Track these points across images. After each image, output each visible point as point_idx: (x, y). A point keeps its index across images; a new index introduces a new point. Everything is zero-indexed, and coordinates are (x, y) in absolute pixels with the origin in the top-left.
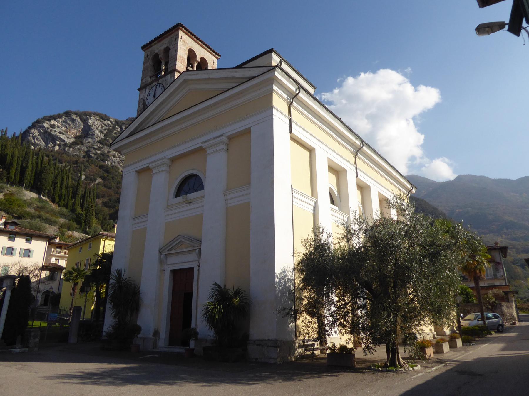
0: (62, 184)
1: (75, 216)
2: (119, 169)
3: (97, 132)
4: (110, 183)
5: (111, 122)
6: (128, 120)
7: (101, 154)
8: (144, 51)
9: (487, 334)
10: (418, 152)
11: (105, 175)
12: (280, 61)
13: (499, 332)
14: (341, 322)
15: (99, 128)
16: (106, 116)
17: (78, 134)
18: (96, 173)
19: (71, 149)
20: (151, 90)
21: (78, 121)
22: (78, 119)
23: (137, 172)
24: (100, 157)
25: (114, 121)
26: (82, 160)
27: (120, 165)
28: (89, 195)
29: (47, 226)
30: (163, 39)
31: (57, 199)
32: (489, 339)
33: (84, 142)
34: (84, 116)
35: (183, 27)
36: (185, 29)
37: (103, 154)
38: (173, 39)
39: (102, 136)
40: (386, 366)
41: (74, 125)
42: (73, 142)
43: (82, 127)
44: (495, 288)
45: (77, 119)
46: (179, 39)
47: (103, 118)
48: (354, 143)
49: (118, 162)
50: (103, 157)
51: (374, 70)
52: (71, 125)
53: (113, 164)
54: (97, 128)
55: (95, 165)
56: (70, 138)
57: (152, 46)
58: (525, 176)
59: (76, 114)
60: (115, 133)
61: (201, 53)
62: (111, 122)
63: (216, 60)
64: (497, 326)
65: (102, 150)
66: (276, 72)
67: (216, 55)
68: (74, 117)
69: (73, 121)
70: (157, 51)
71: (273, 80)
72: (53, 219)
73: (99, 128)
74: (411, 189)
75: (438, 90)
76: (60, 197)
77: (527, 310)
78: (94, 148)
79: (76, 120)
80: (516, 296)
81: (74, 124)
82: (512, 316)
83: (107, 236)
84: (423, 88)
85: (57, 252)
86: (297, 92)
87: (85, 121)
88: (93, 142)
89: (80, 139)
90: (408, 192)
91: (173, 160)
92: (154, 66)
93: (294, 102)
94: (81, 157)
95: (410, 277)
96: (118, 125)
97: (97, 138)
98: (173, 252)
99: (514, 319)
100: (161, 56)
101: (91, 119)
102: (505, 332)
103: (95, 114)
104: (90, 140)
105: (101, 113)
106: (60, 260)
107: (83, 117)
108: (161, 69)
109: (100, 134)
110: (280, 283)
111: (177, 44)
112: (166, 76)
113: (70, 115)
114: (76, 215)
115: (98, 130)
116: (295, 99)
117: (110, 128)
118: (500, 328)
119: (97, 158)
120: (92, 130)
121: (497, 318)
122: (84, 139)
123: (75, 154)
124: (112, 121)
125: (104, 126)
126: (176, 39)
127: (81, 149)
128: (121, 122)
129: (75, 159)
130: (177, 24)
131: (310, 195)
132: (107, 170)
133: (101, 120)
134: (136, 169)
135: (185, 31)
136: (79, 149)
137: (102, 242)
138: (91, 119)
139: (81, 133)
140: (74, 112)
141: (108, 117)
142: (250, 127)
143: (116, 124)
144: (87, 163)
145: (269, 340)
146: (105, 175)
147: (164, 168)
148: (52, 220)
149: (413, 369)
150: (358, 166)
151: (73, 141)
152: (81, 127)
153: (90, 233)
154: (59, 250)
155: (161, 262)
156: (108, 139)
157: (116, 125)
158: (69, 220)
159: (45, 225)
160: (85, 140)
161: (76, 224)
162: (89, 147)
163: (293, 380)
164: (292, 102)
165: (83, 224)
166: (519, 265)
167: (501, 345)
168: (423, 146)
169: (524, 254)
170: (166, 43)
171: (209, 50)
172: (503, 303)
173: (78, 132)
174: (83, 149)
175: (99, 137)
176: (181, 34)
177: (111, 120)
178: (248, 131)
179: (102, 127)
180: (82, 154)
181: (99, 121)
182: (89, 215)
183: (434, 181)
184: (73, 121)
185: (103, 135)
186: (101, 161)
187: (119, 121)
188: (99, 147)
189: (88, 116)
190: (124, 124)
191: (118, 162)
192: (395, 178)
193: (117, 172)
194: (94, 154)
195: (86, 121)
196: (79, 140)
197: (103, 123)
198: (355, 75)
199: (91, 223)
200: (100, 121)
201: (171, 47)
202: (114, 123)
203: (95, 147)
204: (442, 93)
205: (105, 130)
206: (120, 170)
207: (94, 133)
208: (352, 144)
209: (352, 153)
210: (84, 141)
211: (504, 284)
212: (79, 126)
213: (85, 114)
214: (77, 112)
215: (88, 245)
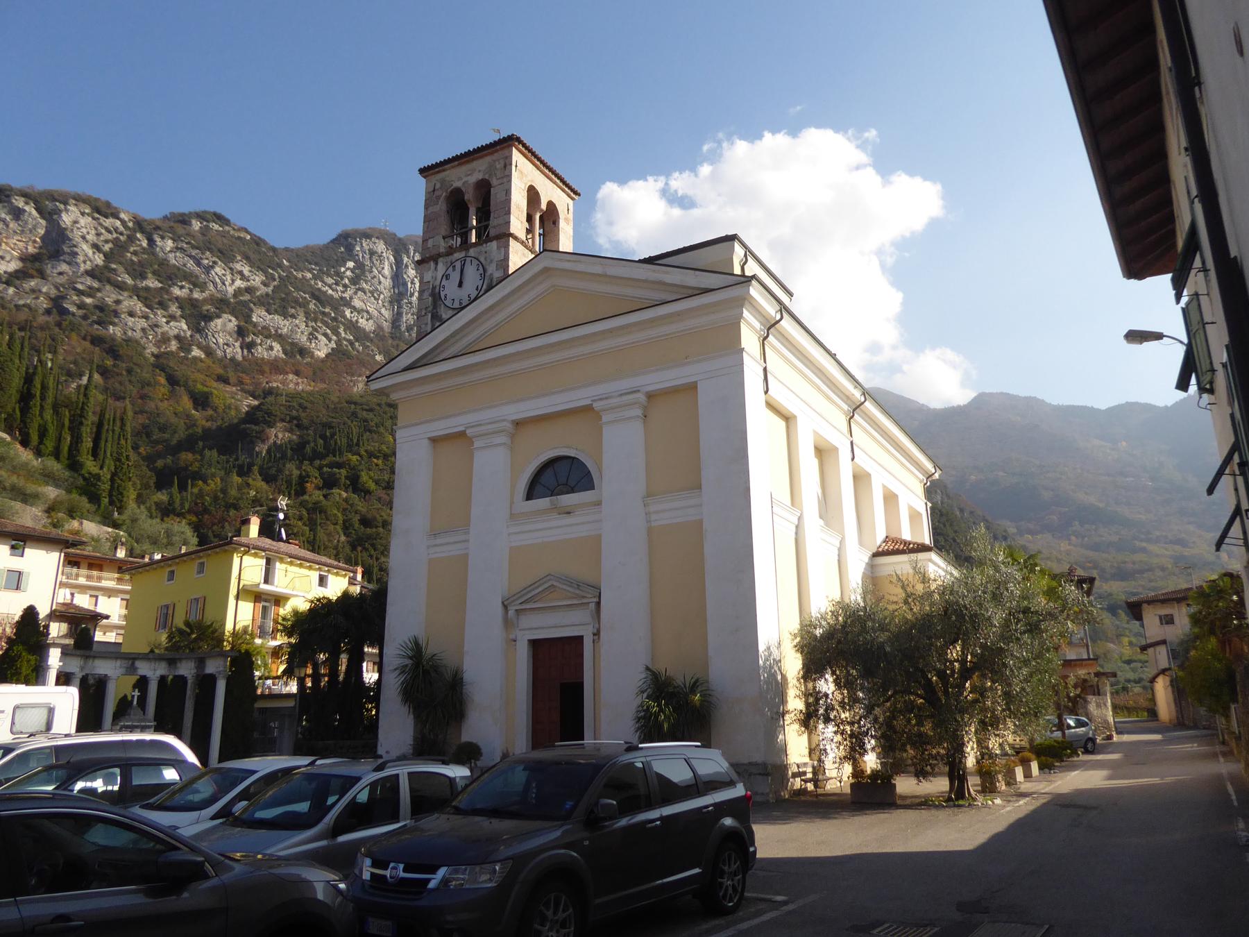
0: (43, 398)
1: (81, 482)
2: (145, 348)
3: (85, 247)
4: (121, 383)
5: (123, 222)
6: (169, 219)
7: (96, 307)
8: (425, 177)
9: (1070, 756)
10: (889, 335)
11: (109, 363)
12: (745, 255)
13: (1087, 752)
14: (426, 747)
15: (91, 237)
16: (108, 204)
17: (31, 250)
18: (85, 356)
19: (11, 290)
20: (451, 268)
21: (30, 214)
22: (30, 209)
23: (434, 440)
24: (93, 314)
25: (130, 220)
26: (42, 319)
27: (148, 338)
28: (111, 428)
29: (18, 505)
30: (473, 160)
31: (35, 438)
32: (1077, 763)
33: (48, 272)
34: (49, 204)
35: (519, 140)
36: (524, 145)
37: (101, 308)
38: (499, 166)
39: (99, 260)
40: (950, 799)
41: (19, 225)
42: (16, 271)
43: (42, 232)
44: (1081, 666)
45: (27, 208)
46: (514, 168)
47: (101, 209)
48: (850, 397)
49: (143, 330)
50: (101, 314)
51: (794, 131)
52: (11, 225)
53: (130, 333)
54: (84, 238)
55: (79, 335)
56: (8, 258)
57: (444, 170)
58: (1127, 402)
59: (26, 195)
60: (135, 253)
61: (550, 192)
62: (123, 222)
63: (571, 202)
64: (1084, 741)
65: (99, 295)
66: (751, 288)
67: (572, 194)
68: (20, 202)
69: (17, 214)
70: (458, 184)
71: (744, 300)
72: (31, 488)
73: (91, 237)
74: (933, 471)
75: (939, 187)
76: (43, 434)
77: (1125, 710)
78: (75, 289)
79: (25, 211)
80: (1113, 679)
81: (20, 223)
82: (1106, 722)
83: (249, 547)
84: (902, 181)
85: (89, 578)
86: (778, 317)
87: (50, 216)
88: (74, 272)
89: (37, 265)
90: (927, 478)
92: (448, 212)
93: (770, 336)
94: (41, 311)
95: (1004, 664)
96: (143, 231)
97: (85, 262)
98: (528, 606)
99: (1110, 730)
100: (469, 196)
101: (67, 211)
102: (1099, 753)
103: (80, 199)
104: (64, 267)
105: (95, 195)
106: (100, 598)
107: (47, 205)
108: (469, 226)
109: (94, 253)
110: (765, 668)
111: (509, 176)
112: (486, 243)
113: (8, 196)
114: (85, 479)
115: (87, 242)
116: (772, 330)
117: (121, 237)
118: (1090, 745)
119: (85, 317)
120: (70, 240)
121: (1083, 726)
122: (47, 264)
123: (21, 302)
124: (126, 219)
125: (103, 231)
126: (505, 166)
127: (40, 291)
128: (150, 222)
129: (22, 316)
130: (508, 136)
131: (788, 502)
132: (112, 349)
133: (97, 215)
135: (523, 149)
136: (33, 291)
137: (236, 560)
138: (67, 211)
139: (40, 248)
140: (20, 191)
141: (116, 208)
142: (696, 382)
143: (137, 227)
144: (57, 330)
145: (750, 764)
146: (109, 363)
147: (502, 439)
148: (28, 492)
149: (993, 803)
150: (855, 439)
151: (18, 268)
152: (39, 231)
153: (122, 525)
154: (75, 570)
155: (508, 624)
156: (114, 266)
157: (136, 232)
158: (69, 491)
159: (13, 503)
160: (49, 266)
161: (87, 500)
162: (63, 285)
163: (829, 818)
164: (768, 336)
165: (106, 501)
166: (1106, 606)
167: (1104, 773)
168: (905, 319)
169: (1117, 583)
170: (479, 171)
171: (561, 184)
172: (1090, 698)
173: (30, 243)
174: (44, 290)
175: (91, 261)
176: (517, 156)
177: (122, 216)
178: (692, 387)
179: (98, 235)
180: (43, 303)
181: (90, 219)
182: (121, 480)
183: (923, 405)
184: (17, 214)
185: (101, 255)
186: (96, 326)
187: (146, 221)
188: (90, 288)
189: (60, 202)
190: (157, 228)
191: (143, 330)
192: (909, 456)
193: (141, 355)
194: (76, 304)
195: (55, 217)
196: (33, 265)
197: (101, 224)
198: (753, 136)
199: (125, 499)
200: (94, 218)
201: (494, 182)
202: (131, 224)
203: (80, 286)
204: (949, 197)
205: (107, 241)
206: (148, 351)
207: (75, 249)
208: (847, 398)
209: (845, 413)
210: (48, 269)
211: (1085, 657)
212: (35, 227)
213: (52, 196)
214: (28, 191)
215: (194, 566)
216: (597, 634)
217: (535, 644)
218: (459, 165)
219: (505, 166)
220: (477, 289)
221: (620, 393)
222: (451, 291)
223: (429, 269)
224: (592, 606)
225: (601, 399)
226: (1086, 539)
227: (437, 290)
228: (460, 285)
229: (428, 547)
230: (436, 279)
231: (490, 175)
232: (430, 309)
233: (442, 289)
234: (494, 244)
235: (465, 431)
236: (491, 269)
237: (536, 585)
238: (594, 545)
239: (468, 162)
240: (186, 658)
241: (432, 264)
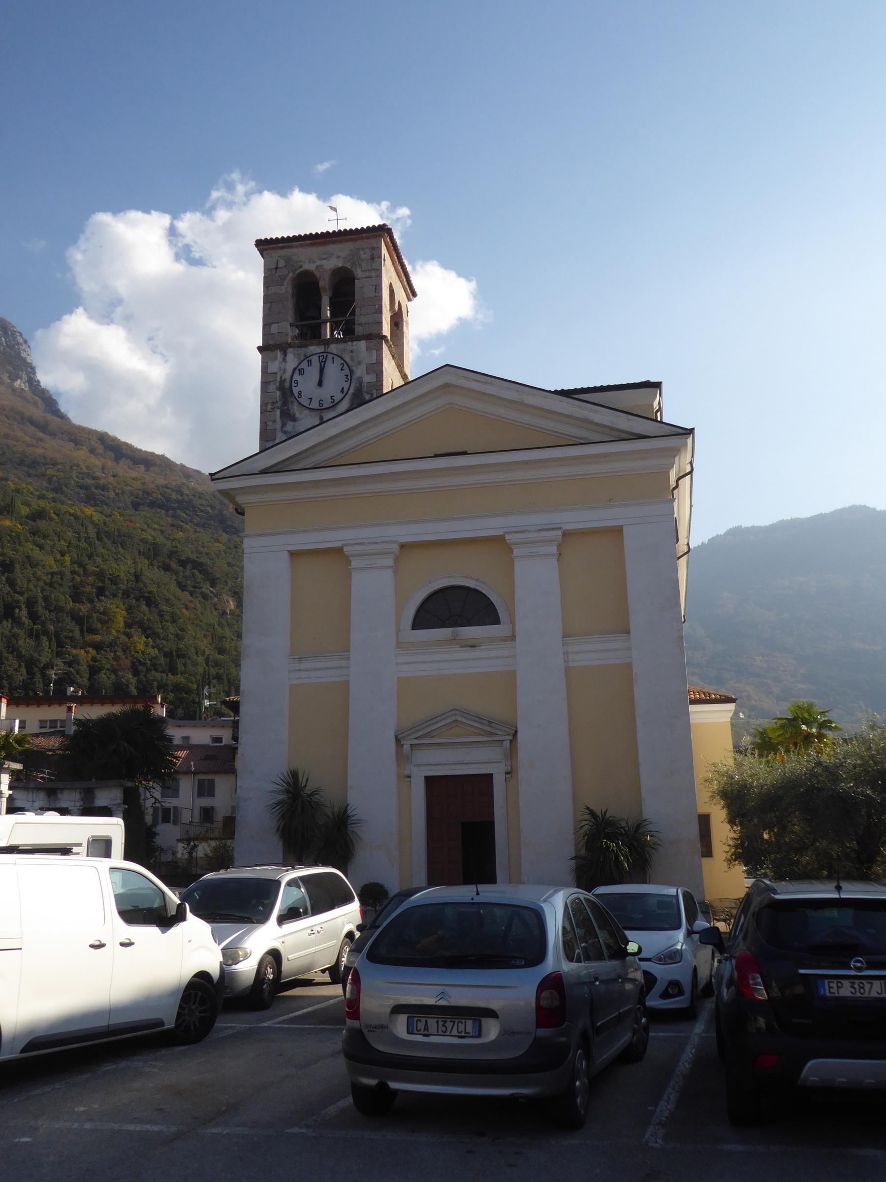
23: (293, 554)
38: (365, 255)
75: (435, 262)
91: (402, 546)
100: (324, 283)
126: (373, 258)
134: (290, 549)
142: (622, 526)
155: (402, 758)
171: (406, 283)
178: (618, 531)
201: (359, 273)
216: (509, 774)
217: (430, 781)
219: (373, 258)
220: (342, 391)
221: (539, 528)
222: (306, 385)
223: (276, 359)
224: (507, 744)
225: (516, 532)
227: (287, 384)
228: (320, 384)
229: (290, 671)
232: (279, 404)
233: (293, 384)
234: (363, 344)
235: (342, 547)
236: (360, 371)
237: (434, 721)
238: (510, 679)
239: (320, 244)
240: (69, 789)
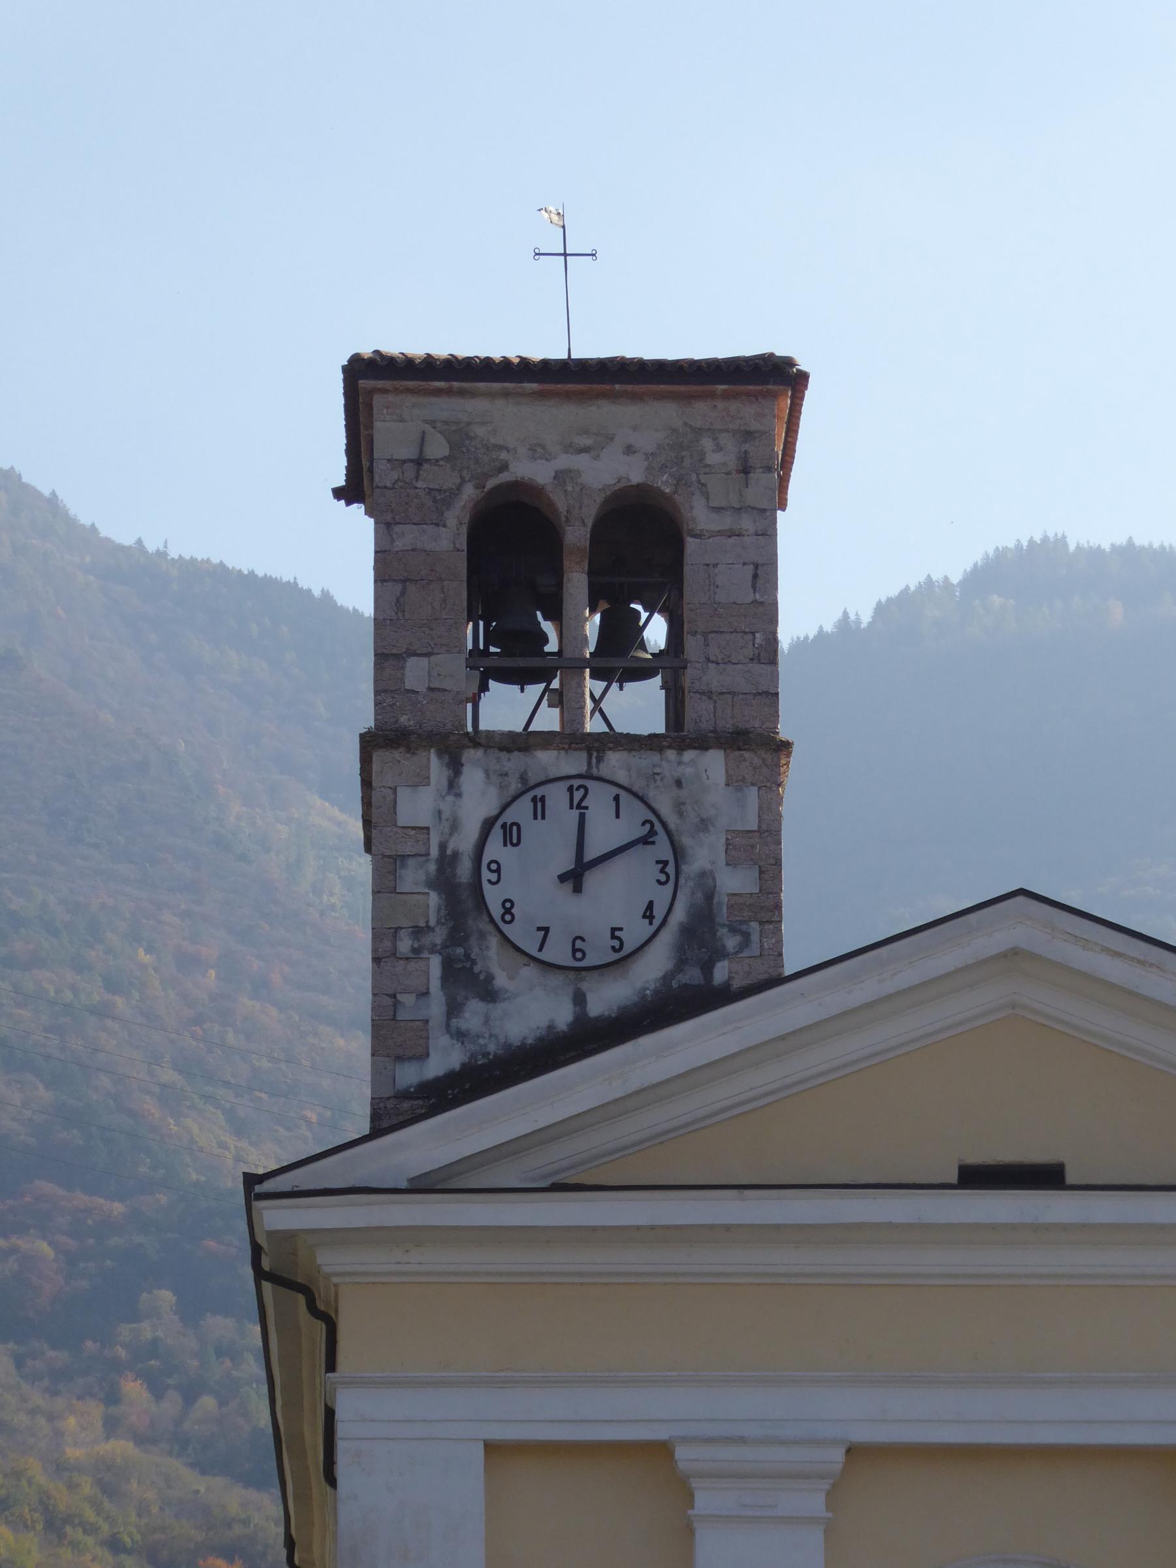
20: (525, 803)
218: (542, 395)
220: (649, 914)
223: (424, 780)
226: (208, 1403)
230: (455, 826)
231: (679, 479)
232: (439, 936)
233: (486, 875)
241: (436, 768)
